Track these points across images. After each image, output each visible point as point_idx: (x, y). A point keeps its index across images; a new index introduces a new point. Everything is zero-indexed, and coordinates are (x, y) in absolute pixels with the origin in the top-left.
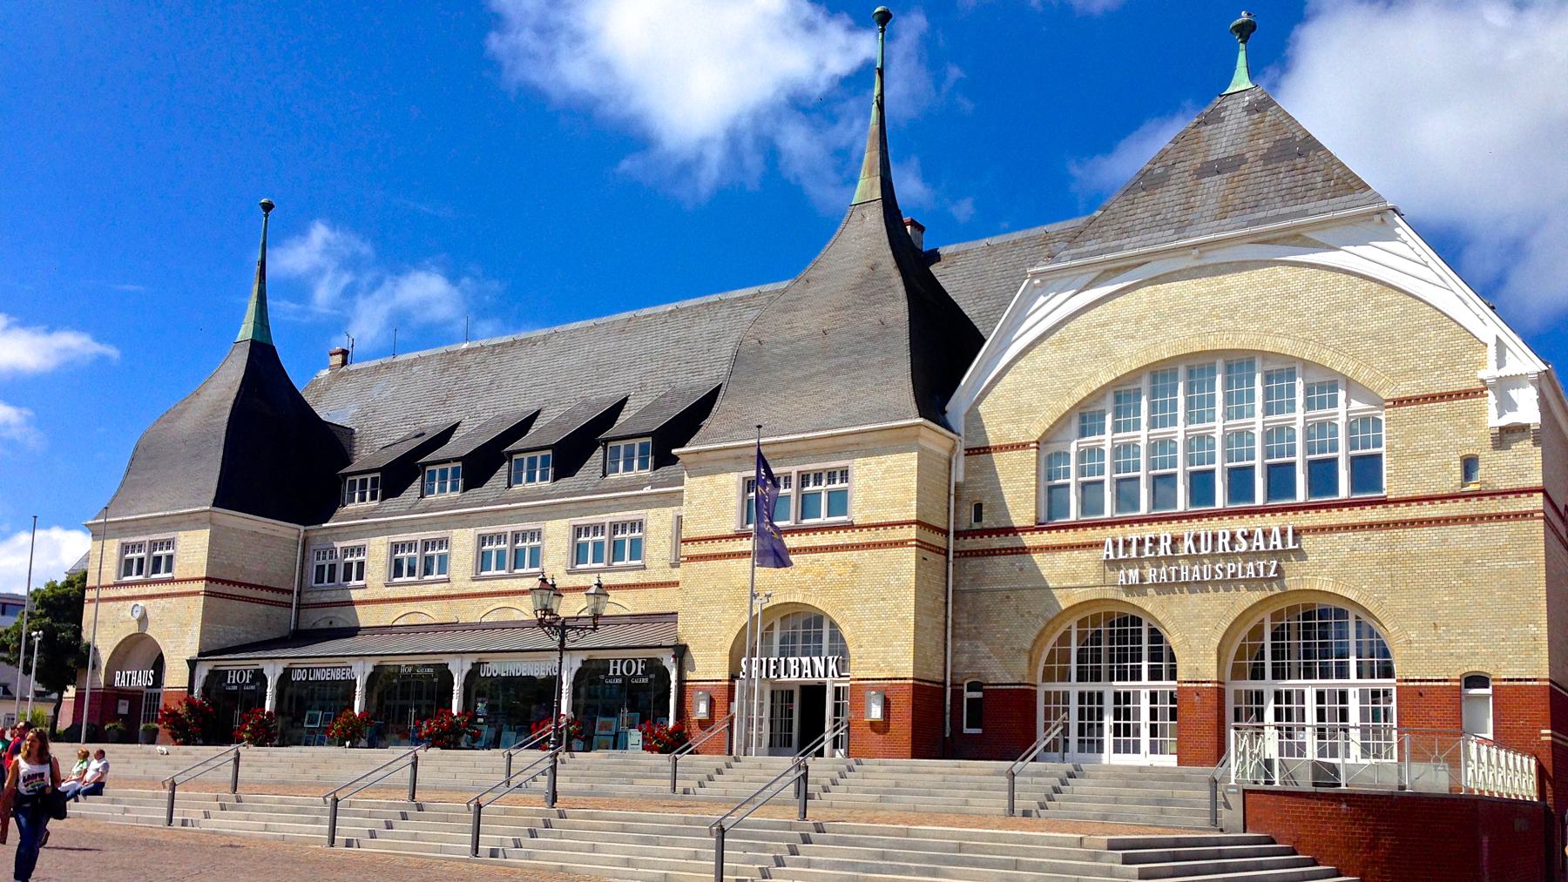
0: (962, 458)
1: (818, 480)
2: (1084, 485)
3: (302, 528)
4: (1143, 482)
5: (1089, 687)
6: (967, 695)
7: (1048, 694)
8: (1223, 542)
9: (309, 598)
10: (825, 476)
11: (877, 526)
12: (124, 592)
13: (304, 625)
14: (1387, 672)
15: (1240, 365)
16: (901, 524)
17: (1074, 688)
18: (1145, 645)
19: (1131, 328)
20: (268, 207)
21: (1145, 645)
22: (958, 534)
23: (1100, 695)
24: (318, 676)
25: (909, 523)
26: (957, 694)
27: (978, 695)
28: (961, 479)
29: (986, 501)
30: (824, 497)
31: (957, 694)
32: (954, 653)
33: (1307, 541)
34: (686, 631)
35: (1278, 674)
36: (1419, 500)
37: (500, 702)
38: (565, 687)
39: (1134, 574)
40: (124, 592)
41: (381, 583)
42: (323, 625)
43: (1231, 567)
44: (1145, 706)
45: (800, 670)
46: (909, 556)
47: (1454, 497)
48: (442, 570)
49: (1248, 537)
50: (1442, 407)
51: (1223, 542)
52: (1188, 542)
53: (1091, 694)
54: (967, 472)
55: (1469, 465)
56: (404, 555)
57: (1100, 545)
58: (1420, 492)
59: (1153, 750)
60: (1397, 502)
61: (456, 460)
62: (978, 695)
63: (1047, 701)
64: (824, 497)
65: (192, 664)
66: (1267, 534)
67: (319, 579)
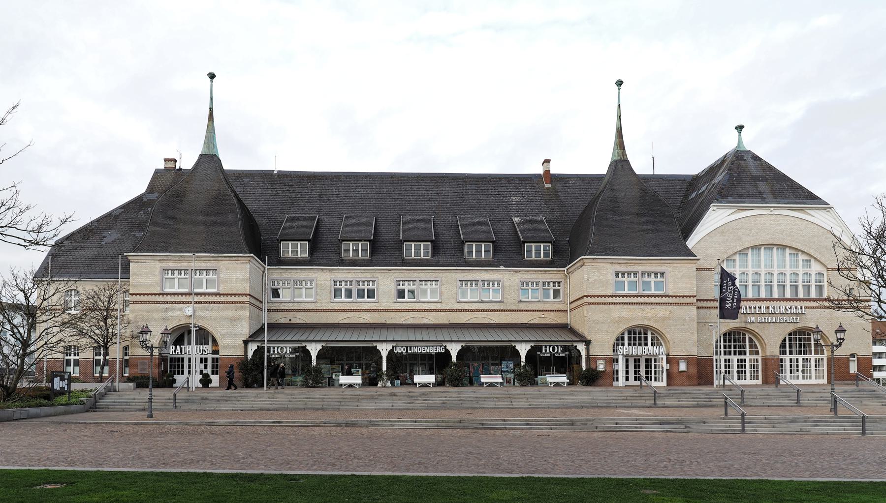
1: (649, 275)
5: (727, 357)
10: (653, 275)
14: (757, 353)
17: (723, 358)
18: (747, 343)
19: (748, 232)
20: (740, 128)
21: (747, 343)
24: (415, 350)
30: (205, 281)
35: (791, 353)
37: (71, 369)
43: (785, 318)
44: (788, 363)
45: (215, 356)
49: (760, 308)
59: (803, 378)
64: (205, 281)
65: (246, 343)
66: (796, 307)
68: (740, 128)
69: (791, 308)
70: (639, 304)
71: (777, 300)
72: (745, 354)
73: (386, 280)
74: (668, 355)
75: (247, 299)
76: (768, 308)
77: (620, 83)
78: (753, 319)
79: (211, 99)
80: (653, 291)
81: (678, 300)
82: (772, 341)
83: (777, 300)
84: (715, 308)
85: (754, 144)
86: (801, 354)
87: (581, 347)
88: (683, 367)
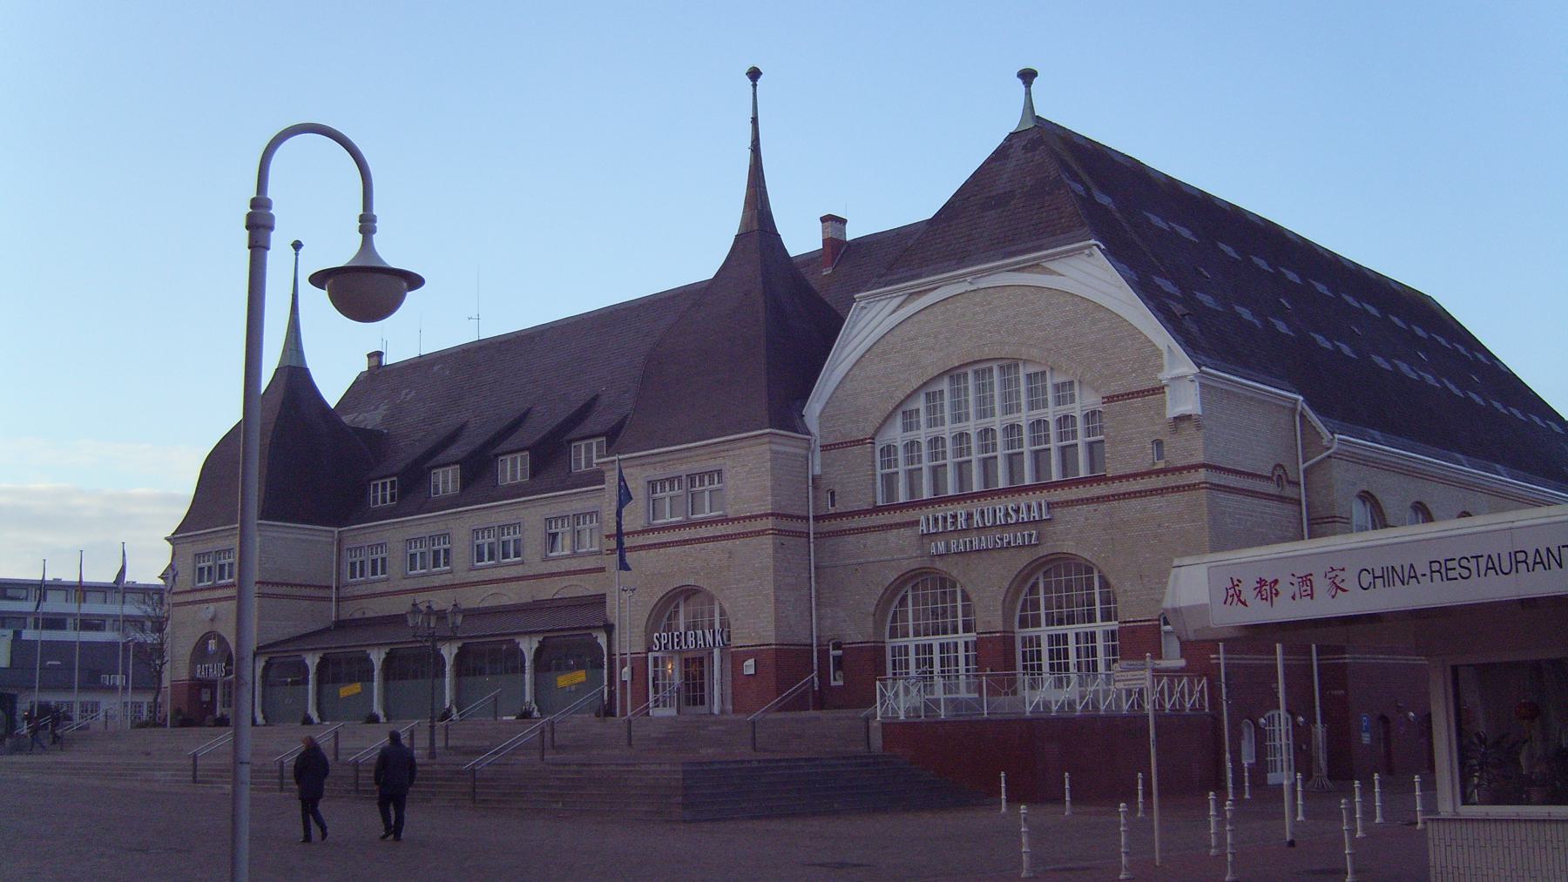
0: (818, 455)
2: (1036, 453)
3: (336, 530)
4: (975, 465)
5: (923, 640)
6: (832, 653)
7: (893, 648)
8: (961, 520)
9: (344, 592)
11: (744, 519)
12: (198, 596)
13: (345, 616)
15: (1009, 367)
16: (761, 516)
17: (1044, 631)
22: (816, 518)
23: (1065, 636)
25: (767, 515)
26: (824, 654)
27: (839, 652)
28: (818, 470)
29: (837, 489)
31: (824, 654)
32: (820, 618)
33: (1058, 512)
34: (613, 611)
36: (1127, 477)
38: (527, 664)
39: (941, 547)
40: (198, 596)
41: (538, 559)
42: (357, 615)
46: (768, 542)
47: (1149, 473)
48: (517, 554)
50: (1138, 402)
51: (961, 520)
52: (977, 517)
53: (1058, 636)
54: (823, 465)
55: (1158, 443)
56: (485, 541)
57: (917, 523)
58: (1128, 471)
60: (1113, 479)
61: (599, 435)
62: (839, 652)
63: (1024, 646)
67: (353, 575)
68: (1027, 76)
69: (1017, 511)
70: (195, 602)
71: (1005, 492)
72: (955, 631)
73: (461, 528)
74: (725, 647)
75: (1202, 475)
76: (970, 516)
77: (754, 74)
78: (941, 547)
79: (755, 121)
80: (707, 513)
81: (734, 527)
82: (987, 594)
83: (1005, 492)
84: (231, 598)
85: (1059, 108)
86: (935, 633)
87: (602, 640)
88: (749, 667)
